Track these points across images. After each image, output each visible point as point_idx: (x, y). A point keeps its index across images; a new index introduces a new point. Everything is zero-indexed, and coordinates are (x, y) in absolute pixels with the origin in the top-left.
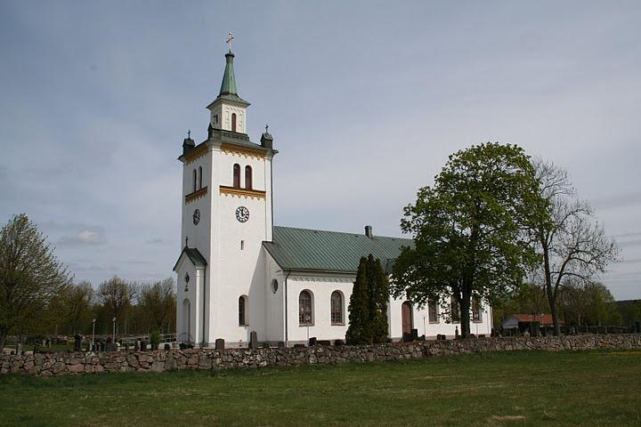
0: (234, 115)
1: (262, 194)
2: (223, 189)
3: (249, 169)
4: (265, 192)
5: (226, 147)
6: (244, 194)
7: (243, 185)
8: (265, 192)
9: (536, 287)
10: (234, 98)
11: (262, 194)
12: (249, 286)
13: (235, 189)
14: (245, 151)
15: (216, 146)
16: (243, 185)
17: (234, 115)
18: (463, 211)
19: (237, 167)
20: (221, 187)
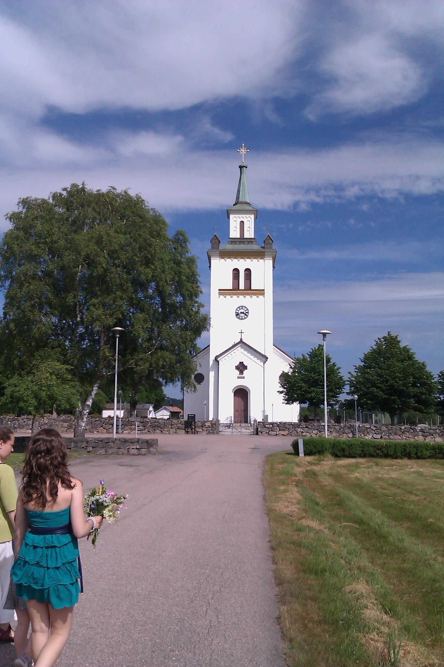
0: (242, 223)
1: (261, 292)
2: (223, 292)
3: (248, 271)
4: (264, 290)
5: (225, 255)
6: (242, 294)
7: (242, 286)
8: (264, 290)
9: (78, 191)
10: (247, 207)
11: (261, 292)
12: (7, 524)
13: (235, 290)
14: (228, 256)
15: (215, 256)
16: (242, 286)
17: (242, 223)
18: (14, 303)
19: (236, 271)
20: (219, 290)
